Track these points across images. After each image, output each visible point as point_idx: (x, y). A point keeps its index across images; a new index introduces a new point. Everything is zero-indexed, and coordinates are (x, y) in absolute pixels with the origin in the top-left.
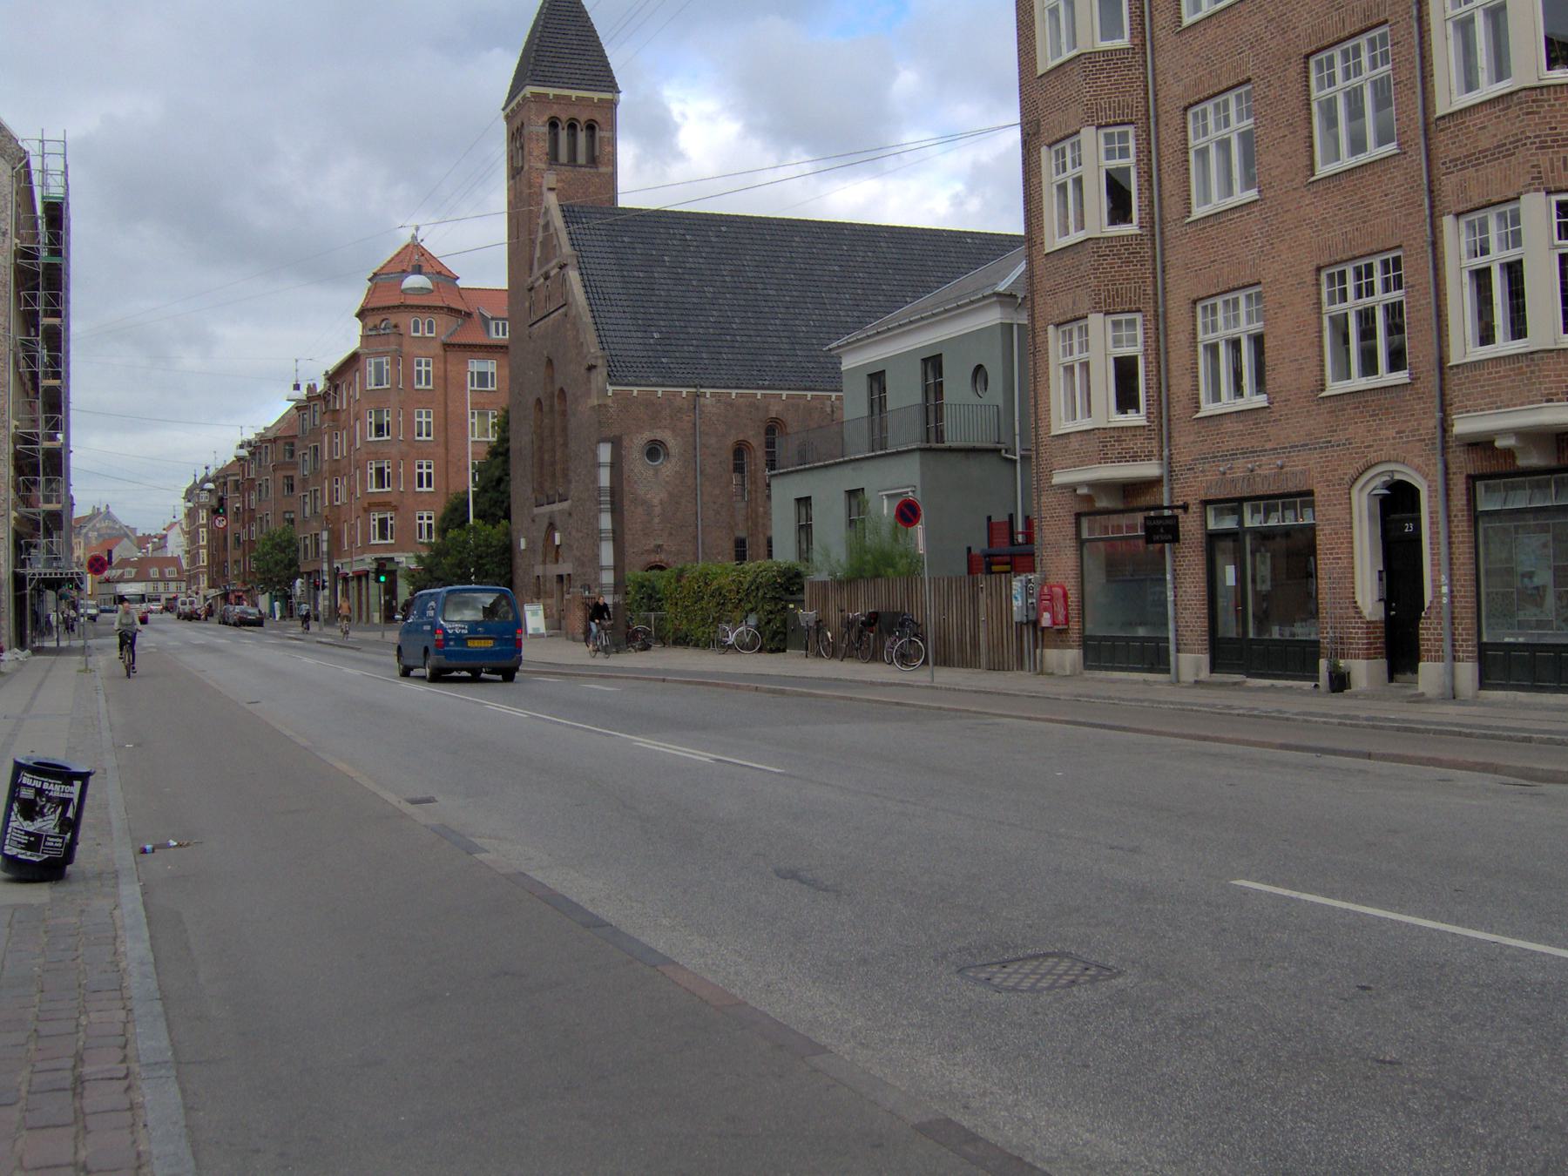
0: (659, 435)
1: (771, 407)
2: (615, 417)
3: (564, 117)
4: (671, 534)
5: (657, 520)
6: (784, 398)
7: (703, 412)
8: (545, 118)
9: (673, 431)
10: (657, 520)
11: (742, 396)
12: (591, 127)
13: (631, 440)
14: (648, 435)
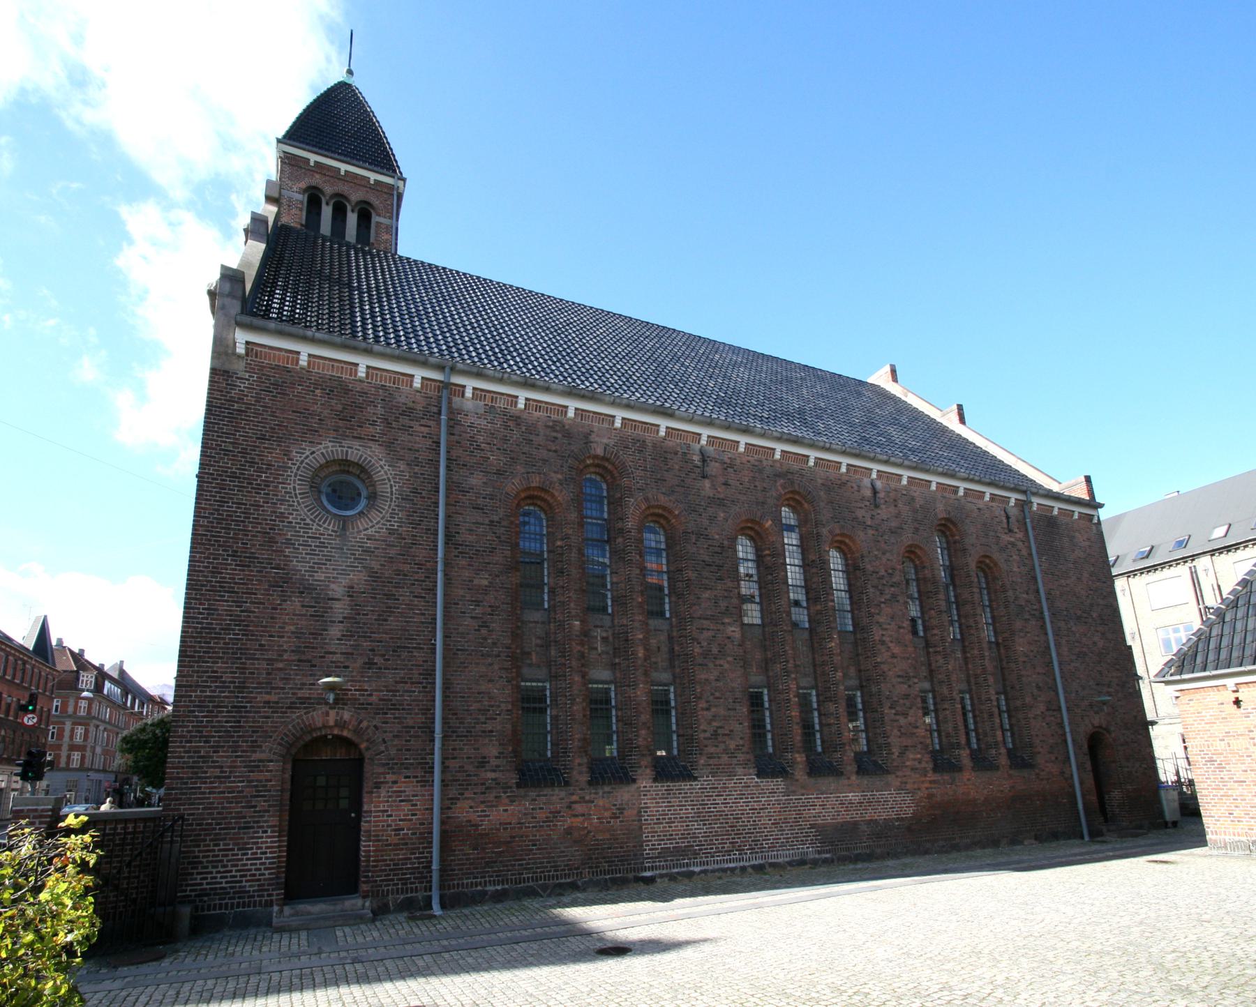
0: (356, 451)
1: (593, 437)
2: (249, 399)
3: (328, 190)
4: (370, 664)
5: (335, 631)
7: (458, 423)
8: (303, 185)
9: (389, 446)
10: (335, 631)
11: (539, 405)
12: (365, 216)
13: (287, 454)
14: (327, 448)
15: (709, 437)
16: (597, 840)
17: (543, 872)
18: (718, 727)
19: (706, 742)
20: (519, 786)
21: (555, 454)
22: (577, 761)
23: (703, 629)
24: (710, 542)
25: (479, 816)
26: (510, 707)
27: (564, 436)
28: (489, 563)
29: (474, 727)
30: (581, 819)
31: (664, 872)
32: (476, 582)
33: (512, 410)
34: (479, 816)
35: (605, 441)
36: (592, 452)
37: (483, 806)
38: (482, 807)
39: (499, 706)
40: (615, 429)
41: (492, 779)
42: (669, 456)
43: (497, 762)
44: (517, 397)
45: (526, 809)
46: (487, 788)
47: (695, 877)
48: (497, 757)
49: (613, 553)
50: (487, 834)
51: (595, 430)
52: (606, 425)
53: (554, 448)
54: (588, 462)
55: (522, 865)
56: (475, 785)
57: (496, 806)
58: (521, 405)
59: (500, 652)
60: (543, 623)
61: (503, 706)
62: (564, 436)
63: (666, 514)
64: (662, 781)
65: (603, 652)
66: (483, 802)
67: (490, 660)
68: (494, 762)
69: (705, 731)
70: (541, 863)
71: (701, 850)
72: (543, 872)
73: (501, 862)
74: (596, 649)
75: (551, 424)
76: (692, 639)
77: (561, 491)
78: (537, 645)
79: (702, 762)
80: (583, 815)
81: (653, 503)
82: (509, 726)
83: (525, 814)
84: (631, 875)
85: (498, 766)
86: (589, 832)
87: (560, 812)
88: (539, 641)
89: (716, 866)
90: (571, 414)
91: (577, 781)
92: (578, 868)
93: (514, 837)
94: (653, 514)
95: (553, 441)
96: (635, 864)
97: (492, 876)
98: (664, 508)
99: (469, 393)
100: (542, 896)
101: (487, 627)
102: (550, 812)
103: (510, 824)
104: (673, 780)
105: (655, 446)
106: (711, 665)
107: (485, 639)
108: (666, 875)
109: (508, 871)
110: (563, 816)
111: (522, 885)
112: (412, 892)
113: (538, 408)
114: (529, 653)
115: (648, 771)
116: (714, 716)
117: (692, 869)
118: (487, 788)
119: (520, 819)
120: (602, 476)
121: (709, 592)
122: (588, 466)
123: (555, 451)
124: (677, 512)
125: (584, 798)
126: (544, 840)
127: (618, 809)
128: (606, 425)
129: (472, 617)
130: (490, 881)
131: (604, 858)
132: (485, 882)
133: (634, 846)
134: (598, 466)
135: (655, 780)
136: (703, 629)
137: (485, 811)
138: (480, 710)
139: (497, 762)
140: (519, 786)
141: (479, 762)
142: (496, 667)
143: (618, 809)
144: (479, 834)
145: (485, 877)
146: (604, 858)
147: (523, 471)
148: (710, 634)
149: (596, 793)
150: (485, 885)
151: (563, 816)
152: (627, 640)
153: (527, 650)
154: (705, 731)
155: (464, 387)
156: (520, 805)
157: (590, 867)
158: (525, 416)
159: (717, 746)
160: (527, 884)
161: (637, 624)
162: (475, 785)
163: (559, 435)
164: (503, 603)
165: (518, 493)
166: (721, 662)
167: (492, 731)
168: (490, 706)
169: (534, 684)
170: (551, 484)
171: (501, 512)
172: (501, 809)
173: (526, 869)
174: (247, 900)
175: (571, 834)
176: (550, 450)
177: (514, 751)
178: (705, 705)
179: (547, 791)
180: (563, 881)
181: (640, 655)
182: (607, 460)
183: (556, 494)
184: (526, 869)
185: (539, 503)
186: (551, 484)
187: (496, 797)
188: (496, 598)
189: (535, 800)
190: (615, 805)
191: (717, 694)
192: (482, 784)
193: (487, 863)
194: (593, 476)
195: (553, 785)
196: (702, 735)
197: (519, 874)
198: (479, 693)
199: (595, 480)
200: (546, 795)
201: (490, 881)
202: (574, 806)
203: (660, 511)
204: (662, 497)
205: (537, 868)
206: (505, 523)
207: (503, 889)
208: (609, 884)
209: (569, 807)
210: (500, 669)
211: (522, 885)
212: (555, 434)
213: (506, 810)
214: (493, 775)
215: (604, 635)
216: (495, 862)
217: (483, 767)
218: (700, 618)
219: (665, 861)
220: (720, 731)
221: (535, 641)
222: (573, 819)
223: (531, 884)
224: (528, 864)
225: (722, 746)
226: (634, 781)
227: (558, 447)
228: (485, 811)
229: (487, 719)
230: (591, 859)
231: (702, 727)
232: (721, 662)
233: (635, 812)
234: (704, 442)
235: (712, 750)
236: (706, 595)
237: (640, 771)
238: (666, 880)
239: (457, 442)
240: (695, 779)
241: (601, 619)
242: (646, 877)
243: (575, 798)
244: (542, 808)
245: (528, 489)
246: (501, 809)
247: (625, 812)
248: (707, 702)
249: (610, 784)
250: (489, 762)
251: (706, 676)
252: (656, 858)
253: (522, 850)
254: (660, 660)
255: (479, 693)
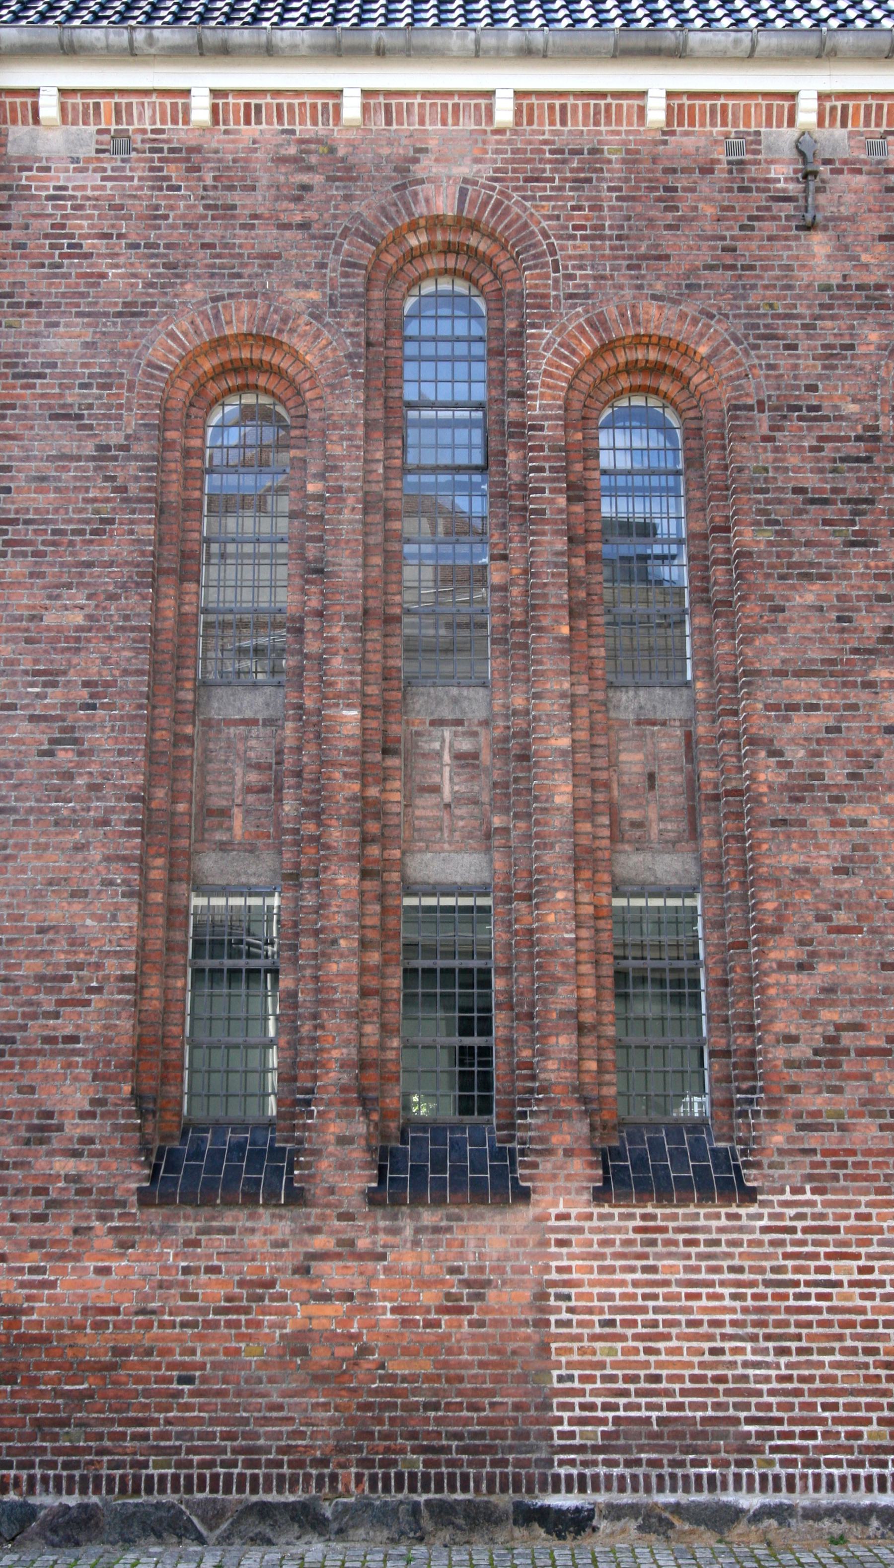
1: (426, 167)
6: (504, 113)
15: (823, 97)
16: (393, 1378)
17: (211, 1464)
18: (839, 1027)
19: (793, 1076)
20: (145, 1199)
21: (299, 235)
22: (335, 1128)
23: (794, 707)
24: (826, 428)
25: (22, 1285)
26: (130, 969)
27: (330, 179)
28: (90, 565)
29: (24, 1028)
30: (340, 1307)
31: (627, 1498)
32: (50, 619)
33: (178, 134)
34: (22, 1285)
35: (465, 170)
36: (420, 210)
37: (36, 1254)
38: (35, 1258)
39: (98, 966)
40: (500, 131)
41: (68, 1178)
42: (681, 181)
43: (87, 1128)
44: (186, 93)
45: (165, 1269)
46: (50, 1204)
47: (741, 1527)
48: (83, 1115)
49: (500, 496)
50: (45, 1339)
51: (432, 144)
52: (467, 124)
53: (298, 218)
54: (413, 242)
55: (145, 1437)
56: (18, 1192)
57: (76, 1258)
58: (201, 113)
59: (112, 810)
60: (269, 722)
61: (112, 967)
62: (330, 179)
63: (671, 361)
64: (623, 1199)
65: (458, 799)
66: (35, 1244)
67: (78, 836)
68: (75, 1128)
69: (791, 1039)
70: (203, 1436)
71: (768, 1436)
72: (211, 1464)
73: (81, 1424)
74: (436, 789)
75: (292, 151)
76: (751, 741)
77: (317, 336)
78: (248, 789)
79: (778, 1140)
80: (350, 1297)
81: (619, 331)
82: (125, 1024)
83: (161, 1285)
84: (504, 1500)
85: (84, 1140)
86: (365, 1350)
87: (271, 1284)
88: (253, 777)
89: (824, 1499)
90: (352, 109)
91: (331, 1191)
92: (323, 1462)
93: (126, 1352)
94: (630, 368)
95: (298, 199)
96: (518, 1464)
97: (52, 1465)
98: (663, 343)
99: (49, 108)
100: (201, 1540)
101: (76, 741)
102: (242, 1284)
103: (116, 1311)
104: (664, 1197)
105: (631, 158)
106: (820, 822)
107: (69, 776)
108: (633, 1510)
109: (102, 1452)
110: (283, 1297)
111: (143, 1498)
112: (149, 1491)
113: (251, 114)
114: (225, 813)
115: (577, 1165)
116: (829, 990)
117: (729, 1497)
118: (50, 1204)
119: (147, 1298)
120: (467, 277)
121: (817, 586)
122: (413, 255)
123: (304, 226)
124: (703, 350)
125: (351, 1243)
126: (215, 1366)
127: (467, 1284)
128: (467, 124)
129: (32, 718)
130: (45, 1479)
131: (413, 1436)
132: (31, 1479)
133: (517, 1407)
134: (449, 249)
135: (600, 1196)
136: (794, 707)
137: (40, 1270)
138: (41, 978)
139: (87, 1128)
140: (145, 1199)
141: (31, 1128)
142: (95, 854)
143: (467, 1284)
144: (20, 1338)
145: (31, 1465)
146: (413, 1436)
147: (201, 295)
148: (819, 720)
149: (394, 1231)
150: (31, 1490)
151: (283, 1297)
152: (524, 757)
153: (217, 802)
154: (791, 1039)
155: (34, 92)
156: (147, 1257)
157: (362, 1463)
158: (215, 141)
159: (838, 1090)
160: (156, 1498)
161: (551, 706)
162: (18, 1192)
163: (316, 179)
164: (126, 672)
165: (190, 360)
166: (860, 811)
167: (74, 1039)
168: (69, 966)
169: (237, 901)
170: (285, 320)
171: (132, 421)
172: (91, 1265)
173: (158, 1450)
174: (38, 1472)
175: (304, 1352)
176: (287, 226)
177: (137, 1096)
178: (792, 954)
179: (229, 1218)
180: (273, 1497)
181: (558, 800)
182: (474, 226)
183: (301, 346)
184: (158, 1450)
185: (262, 381)
186: (285, 320)
187: (76, 1231)
188: (105, 661)
189: (196, 1243)
190: (454, 1270)
191: (842, 917)
192: (38, 1191)
193: (38, 1423)
194: (445, 285)
195: (250, 1200)
196: (779, 1053)
197: (137, 1465)
198: (42, 930)
199: (454, 296)
200: (230, 1231)
201: (45, 1479)
202: (317, 1267)
203: (653, 355)
204: (651, 311)
205: (191, 1450)
206: (141, 449)
207: (83, 1507)
208: (427, 1523)
209: (303, 1270)
210: (107, 859)
211: (143, 1498)
212: (304, 178)
213: (104, 1271)
214: (64, 1166)
215: (465, 745)
216: (64, 1423)
217: (41, 1142)
218: (783, 673)
219: (628, 1464)
220: (847, 1039)
221: (243, 776)
222: (315, 1308)
223: (170, 1497)
224: (165, 1436)
225: (855, 1091)
226: (523, 1195)
227: (312, 214)
228: (40, 1270)
229: (61, 1003)
230: (370, 1435)
231: (779, 1027)
232: (860, 811)
233: (527, 1294)
234: (807, 115)
235: (818, 1101)
236: (809, 595)
237: (546, 1166)
238: (632, 1525)
239: (16, 246)
240: (749, 1196)
241: (455, 701)
242: (560, 1512)
243: (321, 1242)
244: (216, 1270)
245: (222, 342)
246: (91, 1265)
247: (491, 1294)
248: (801, 943)
249: (439, 1202)
250: (60, 1128)
251: (798, 860)
252: (596, 1449)
253: (147, 1393)
254: (653, 814)
255: (42, 930)
